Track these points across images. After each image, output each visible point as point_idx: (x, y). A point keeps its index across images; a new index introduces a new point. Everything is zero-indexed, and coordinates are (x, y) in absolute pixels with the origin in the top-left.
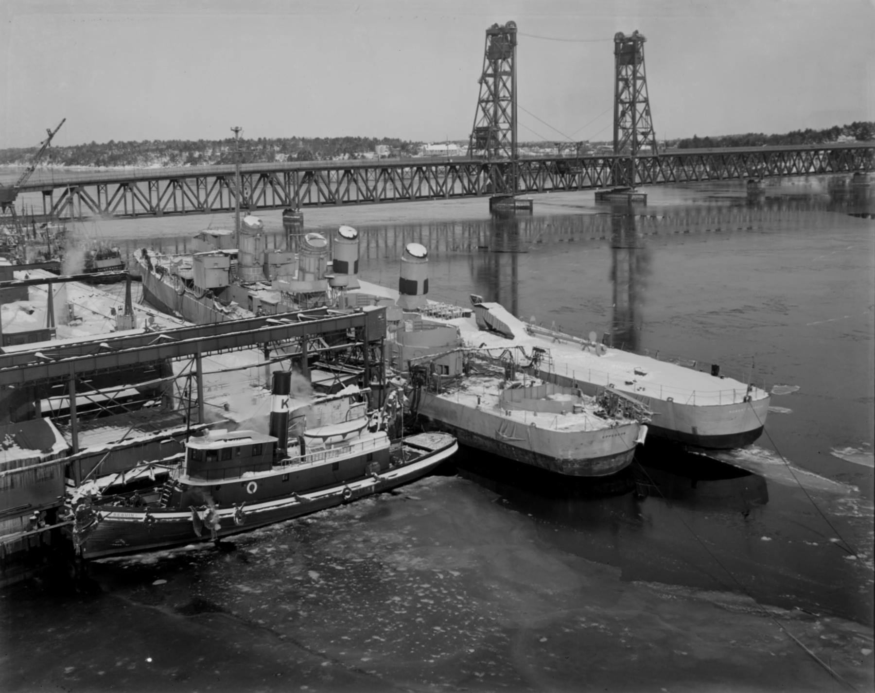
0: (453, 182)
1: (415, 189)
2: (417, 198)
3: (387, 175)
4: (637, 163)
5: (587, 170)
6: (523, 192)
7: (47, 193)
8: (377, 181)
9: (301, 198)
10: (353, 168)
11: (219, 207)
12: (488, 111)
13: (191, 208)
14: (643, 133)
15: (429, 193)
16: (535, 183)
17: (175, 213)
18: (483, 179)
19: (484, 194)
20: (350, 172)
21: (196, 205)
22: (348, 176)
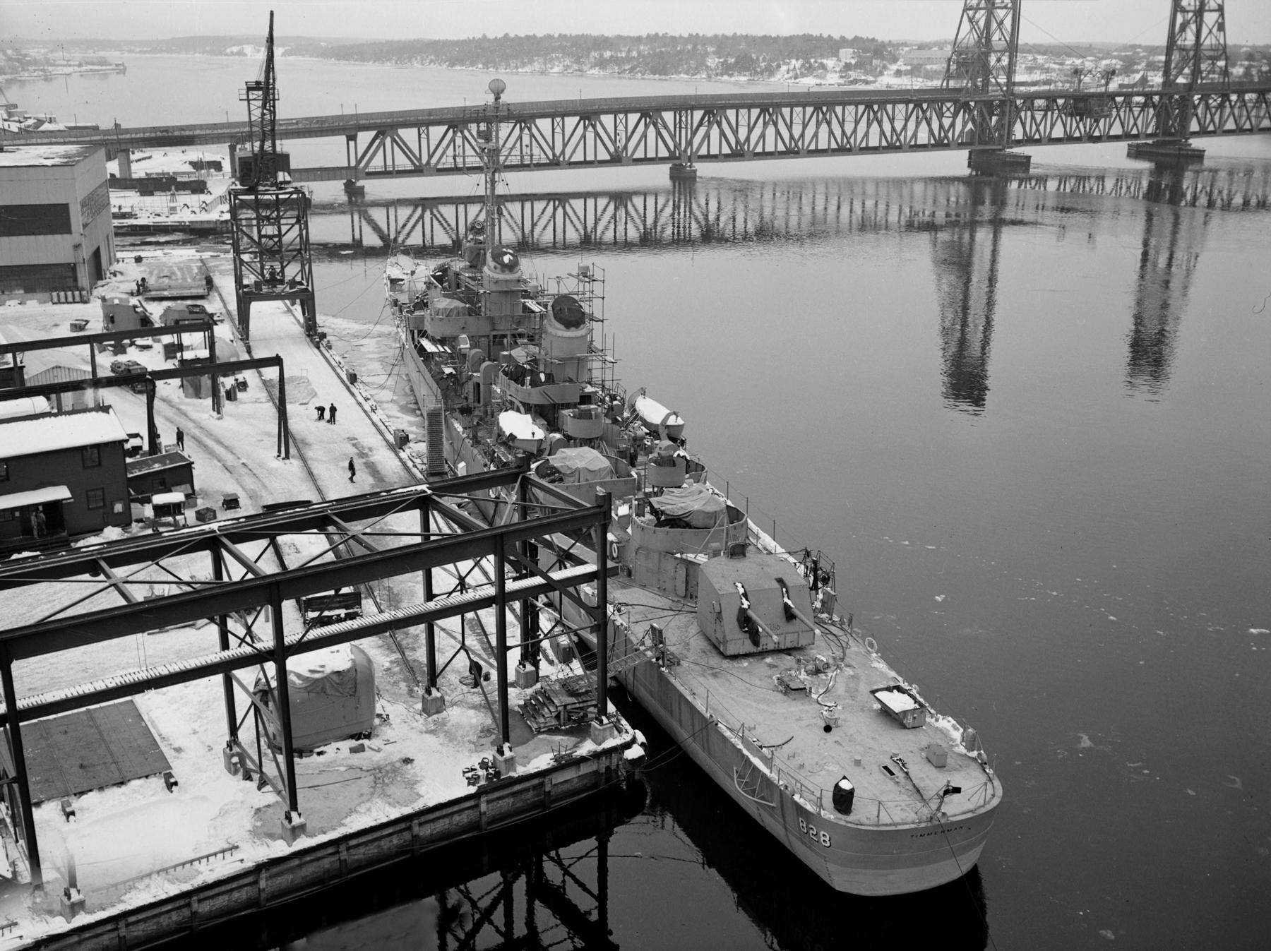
1: (910, 134)
2: (912, 147)
4: (1197, 102)
5: (1118, 111)
6: (1019, 143)
7: (352, 138)
9: (694, 150)
11: (643, 156)
12: (977, 23)
13: (544, 161)
14: (1209, 58)
15: (929, 140)
16: (1038, 130)
17: (585, 163)
18: (961, 125)
19: (961, 145)
21: (551, 157)
22: (818, 116)
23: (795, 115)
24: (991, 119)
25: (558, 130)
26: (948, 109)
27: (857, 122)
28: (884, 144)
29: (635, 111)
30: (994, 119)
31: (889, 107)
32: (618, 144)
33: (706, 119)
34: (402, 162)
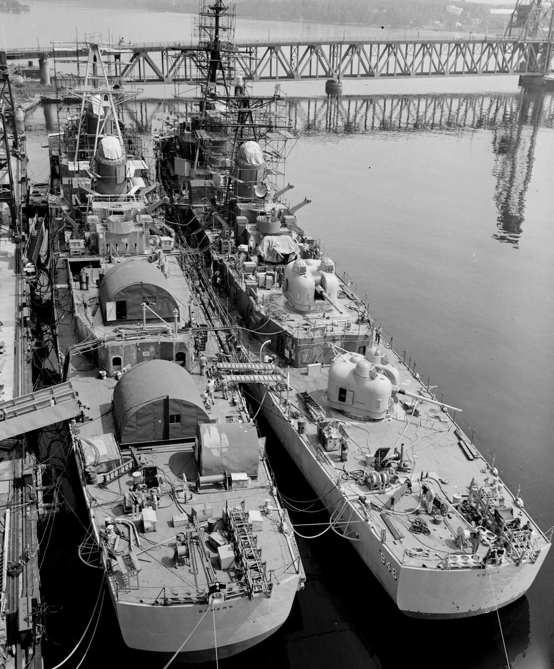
0: (489, 57)
3: (459, 49)
8: (482, 53)
10: (429, 42)
11: (349, 73)
20: (391, 46)
23: (476, 48)
24: (537, 55)
25: (294, 55)
26: (510, 48)
27: (449, 55)
28: (466, 70)
29: (263, 45)
30: (539, 55)
31: (471, 46)
32: (292, 66)
33: (351, 50)
34: (150, 73)
